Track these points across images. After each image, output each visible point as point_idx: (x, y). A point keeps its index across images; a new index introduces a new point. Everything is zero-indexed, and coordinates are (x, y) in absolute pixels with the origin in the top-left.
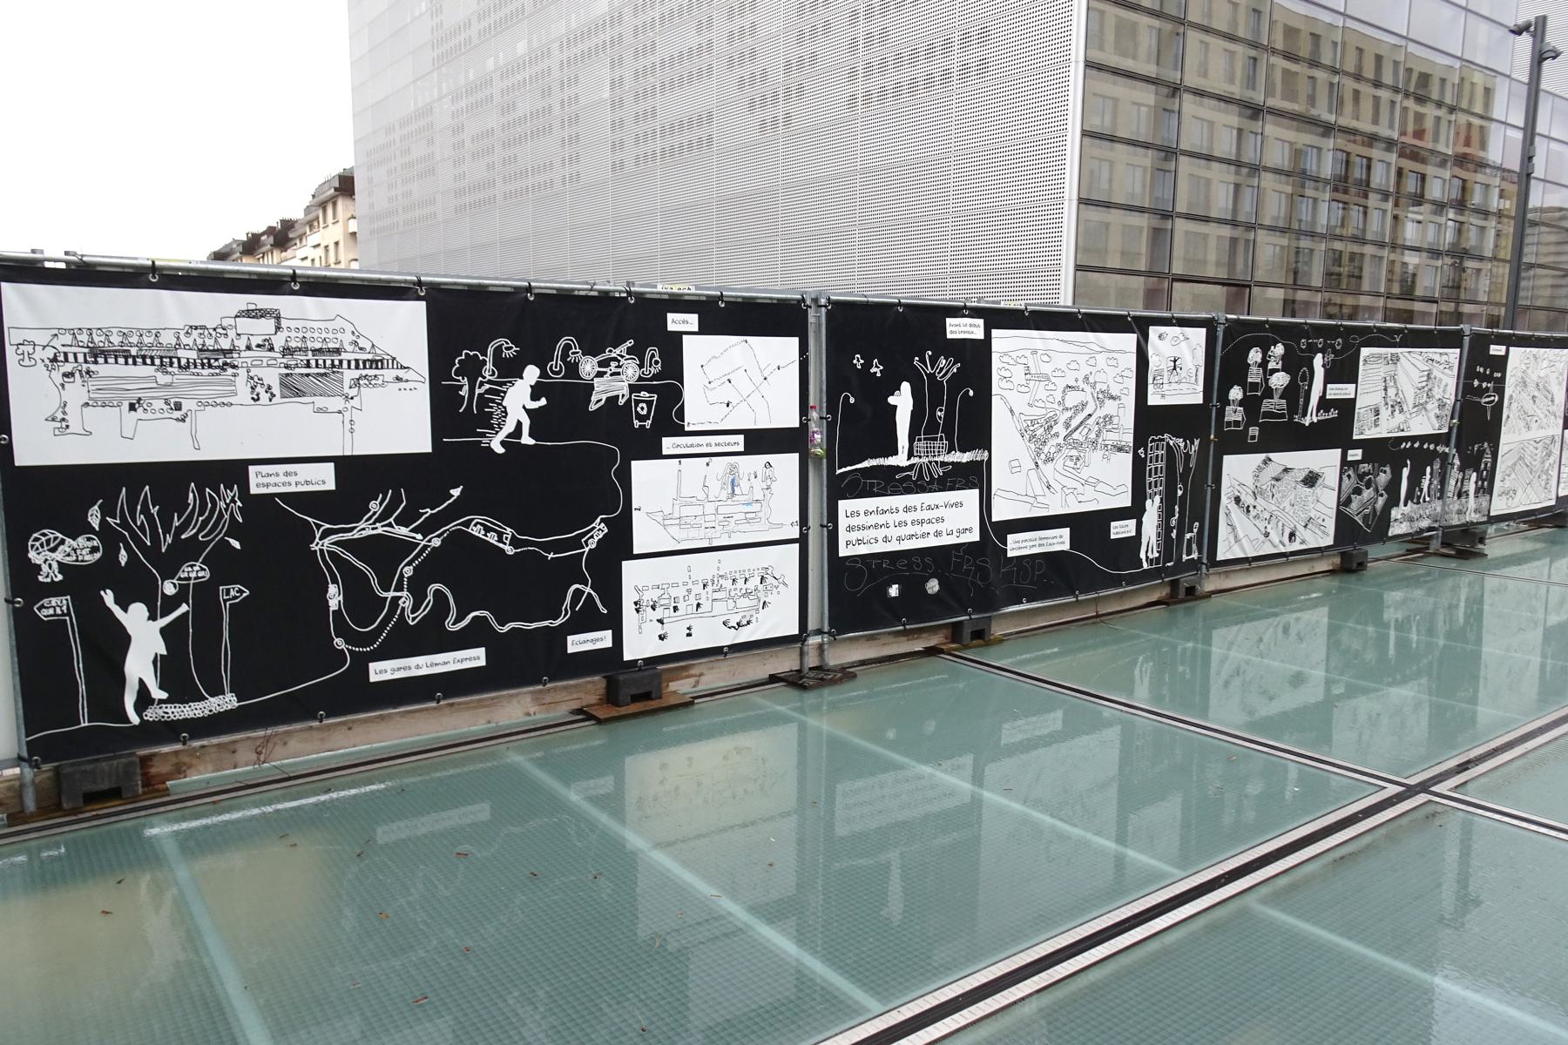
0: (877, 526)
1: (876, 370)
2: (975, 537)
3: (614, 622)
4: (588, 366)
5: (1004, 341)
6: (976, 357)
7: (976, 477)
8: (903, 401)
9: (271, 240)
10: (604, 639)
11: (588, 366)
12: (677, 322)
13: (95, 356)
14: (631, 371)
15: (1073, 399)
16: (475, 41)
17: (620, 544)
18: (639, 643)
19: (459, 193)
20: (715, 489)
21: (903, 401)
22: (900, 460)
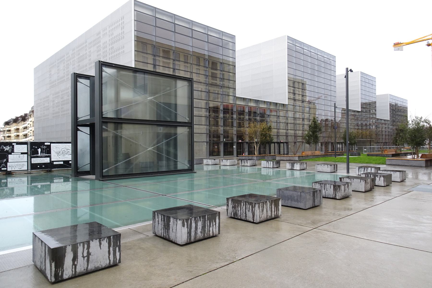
0: (35, 161)
1: (36, 147)
2: (49, 162)
3: (7, 167)
4: (4, 148)
5: (52, 144)
6: (49, 147)
7: (50, 157)
8: (39, 150)
9: (21, 119)
10: (6, 169)
11: (4, 148)
12: (13, 144)
13: (297, 200)
14: (9, 148)
15: (63, 150)
16: (66, 80)
17: (7, 161)
18: (9, 169)
19: (53, 114)
20: (18, 157)
21: (39, 150)
22: (39, 155)
